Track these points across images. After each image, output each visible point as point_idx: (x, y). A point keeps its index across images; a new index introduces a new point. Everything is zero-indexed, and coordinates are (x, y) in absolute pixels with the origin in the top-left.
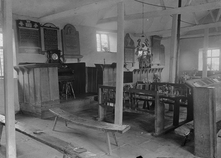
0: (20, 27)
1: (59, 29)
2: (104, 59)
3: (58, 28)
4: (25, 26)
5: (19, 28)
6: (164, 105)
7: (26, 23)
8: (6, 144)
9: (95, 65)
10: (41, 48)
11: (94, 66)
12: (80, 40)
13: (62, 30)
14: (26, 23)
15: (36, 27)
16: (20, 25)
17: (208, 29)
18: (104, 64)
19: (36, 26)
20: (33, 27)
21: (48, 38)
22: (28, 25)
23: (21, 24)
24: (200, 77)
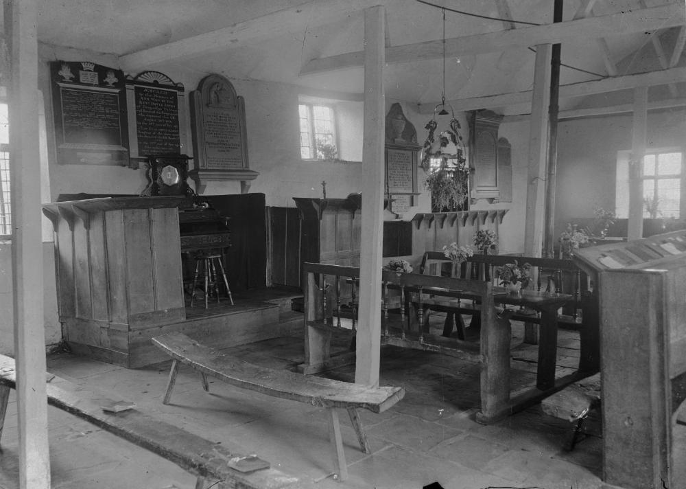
1: (182, 89)
4: (76, 80)
5: (59, 87)
7: (81, 72)
11: (293, 204)
14: (81, 72)
15: (111, 85)
19: (111, 79)
22: (88, 77)
23: (66, 73)
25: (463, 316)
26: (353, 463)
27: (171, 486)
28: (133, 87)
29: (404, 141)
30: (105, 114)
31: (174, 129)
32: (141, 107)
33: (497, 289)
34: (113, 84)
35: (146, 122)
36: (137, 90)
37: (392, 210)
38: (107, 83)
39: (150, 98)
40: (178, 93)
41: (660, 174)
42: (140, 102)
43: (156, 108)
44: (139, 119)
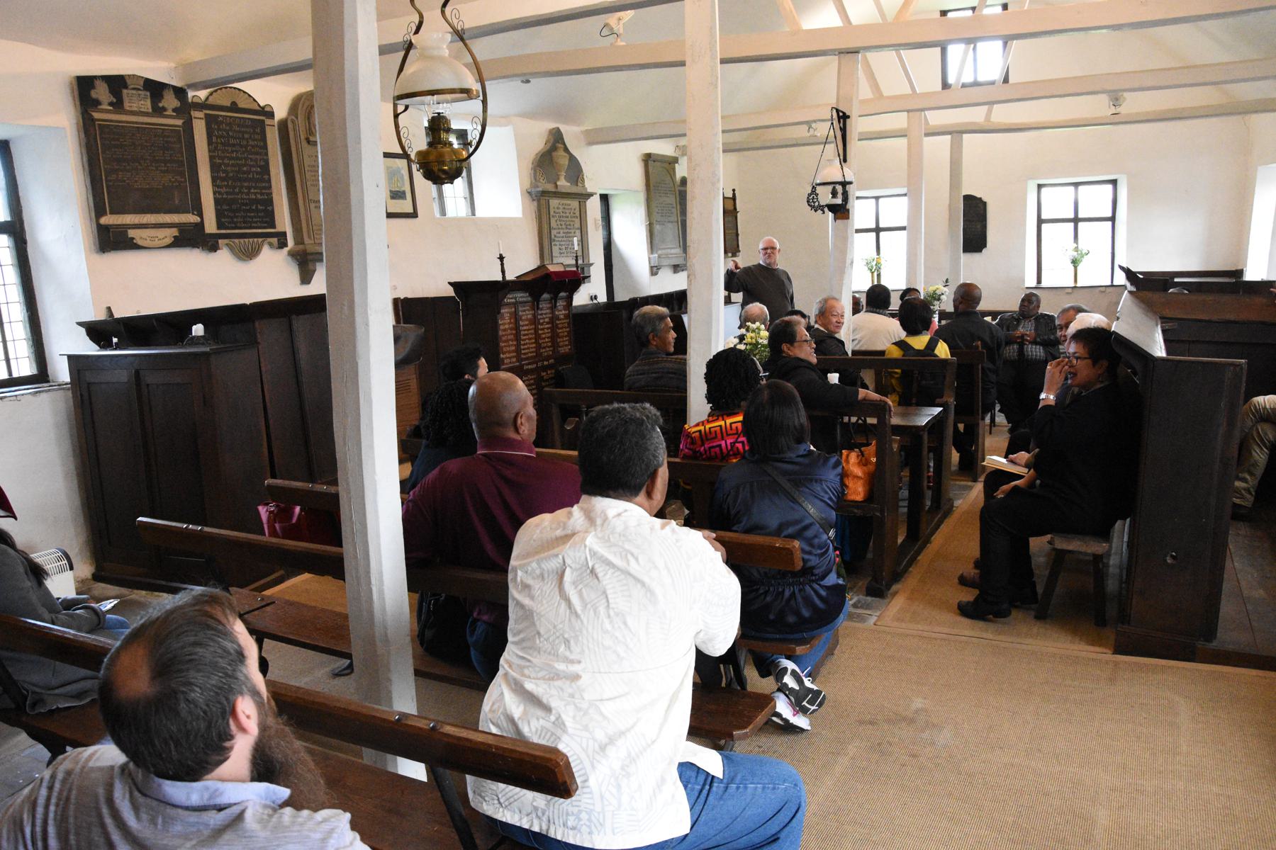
0: (96, 115)
1: (271, 115)
2: (501, 258)
3: (267, 109)
4: (118, 105)
5: (93, 120)
6: (817, 351)
7: (125, 91)
8: (685, 259)
9: (451, 289)
10: (197, 219)
11: (450, 292)
12: (514, 145)
13: (283, 125)
14: (125, 91)
15: (169, 112)
16: (97, 103)
17: (848, 388)
18: (500, 278)
19: (170, 102)
20: (158, 111)
21: (227, 165)
22: (138, 102)
23: (102, 93)
24: (774, 719)
25: (871, 450)
26: (844, 762)
27: (950, 15)
28: (200, 114)
29: (852, 749)
30: (165, 162)
31: (263, 180)
32: (216, 148)
33: (839, 576)
34: (174, 110)
35: (224, 171)
36: (210, 120)
37: (448, 9)
38: (164, 109)
39: (227, 132)
40: (268, 122)
41: (874, 234)
42: (214, 139)
43: (237, 148)
44: (214, 168)
